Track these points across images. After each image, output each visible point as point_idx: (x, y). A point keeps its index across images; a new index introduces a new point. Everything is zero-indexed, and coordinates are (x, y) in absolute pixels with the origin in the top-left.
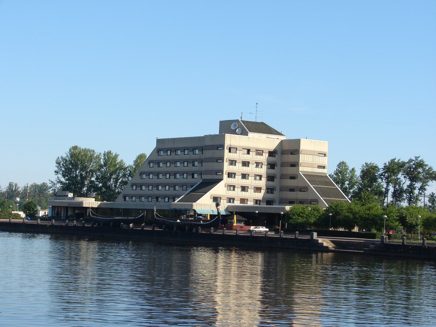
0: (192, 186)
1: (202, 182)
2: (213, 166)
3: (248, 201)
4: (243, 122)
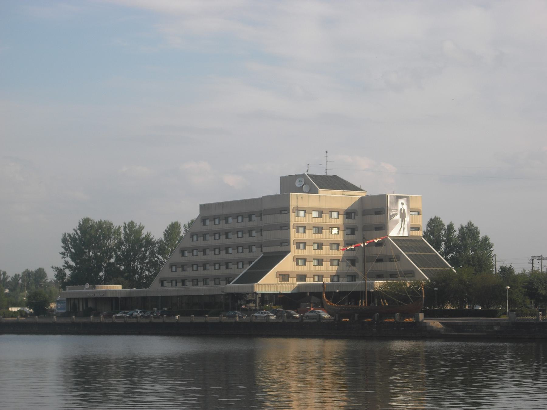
0: (250, 263)
1: (262, 257)
2: (279, 235)
3: (289, 277)
4: (310, 176)
